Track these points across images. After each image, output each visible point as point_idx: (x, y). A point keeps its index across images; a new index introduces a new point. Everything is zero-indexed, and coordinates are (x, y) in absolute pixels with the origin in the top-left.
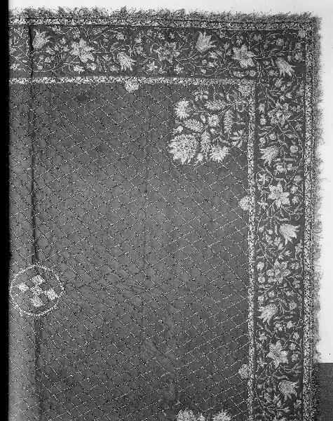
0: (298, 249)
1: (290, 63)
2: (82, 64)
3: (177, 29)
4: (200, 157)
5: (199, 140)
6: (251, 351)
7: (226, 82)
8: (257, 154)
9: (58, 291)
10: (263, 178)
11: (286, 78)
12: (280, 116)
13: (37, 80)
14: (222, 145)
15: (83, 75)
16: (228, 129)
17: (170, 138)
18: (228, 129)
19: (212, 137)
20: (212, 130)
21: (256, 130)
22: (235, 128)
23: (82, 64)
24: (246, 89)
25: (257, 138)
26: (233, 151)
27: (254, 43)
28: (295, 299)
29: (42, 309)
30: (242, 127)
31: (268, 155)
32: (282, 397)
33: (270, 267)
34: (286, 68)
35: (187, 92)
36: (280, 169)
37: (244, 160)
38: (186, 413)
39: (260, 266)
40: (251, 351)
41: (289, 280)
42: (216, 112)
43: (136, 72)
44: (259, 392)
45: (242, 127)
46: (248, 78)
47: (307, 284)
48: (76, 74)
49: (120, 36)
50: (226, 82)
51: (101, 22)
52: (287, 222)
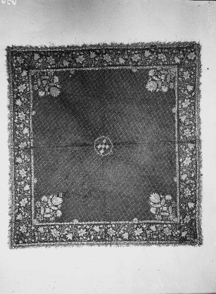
0: (119, 239)
1: (186, 236)
2: (183, 161)
3: (154, 48)
4: (58, 86)
5: (158, 204)
6: (83, 223)
7: (178, 214)
8: (152, 224)
9: (103, 154)
10: (27, 121)
11: (180, 235)
12: (167, 232)
13: (177, 145)
14: (156, 212)
15: (179, 162)
16: (162, 214)
17: (158, 193)
18: (162, 214)
19: (159, 208)
20: (161, 208)
21: (161, 224)
22: (162, 216)
23: (183, 161)
24: (176, 220)
25: (159, 224)
26: (154, 216)
27: (192, 223)
28: (102, 239)
29: (97, 148)
30: (163, 218)
31: (153, 228)
32: (67, 234)
33: (113, 229)
34: (184, 234)
35: (174, 198)
36: (22, 126)
37: (151, 219)
38: (62, 200)
39: (114, 226)
40: (83, 223)
41: (108, 236)
42: (168, 209)
43: (180, 180)
44: (68, 226)
45: (163, 218)
46: (180, 221)
47: (14, 198)
48: (179, 159)
49: (193, 175)
50: (178, 214)
51: (198, 168)
52: (129, 234)
